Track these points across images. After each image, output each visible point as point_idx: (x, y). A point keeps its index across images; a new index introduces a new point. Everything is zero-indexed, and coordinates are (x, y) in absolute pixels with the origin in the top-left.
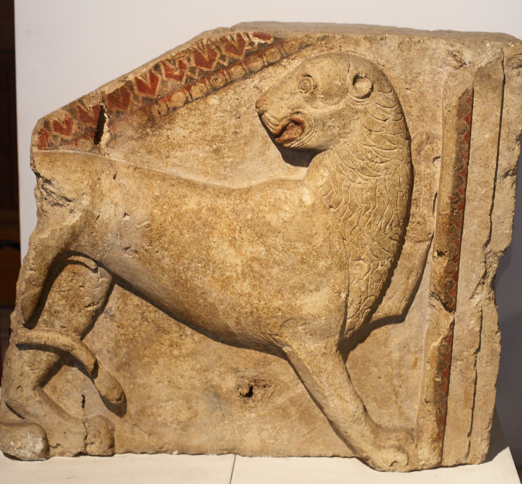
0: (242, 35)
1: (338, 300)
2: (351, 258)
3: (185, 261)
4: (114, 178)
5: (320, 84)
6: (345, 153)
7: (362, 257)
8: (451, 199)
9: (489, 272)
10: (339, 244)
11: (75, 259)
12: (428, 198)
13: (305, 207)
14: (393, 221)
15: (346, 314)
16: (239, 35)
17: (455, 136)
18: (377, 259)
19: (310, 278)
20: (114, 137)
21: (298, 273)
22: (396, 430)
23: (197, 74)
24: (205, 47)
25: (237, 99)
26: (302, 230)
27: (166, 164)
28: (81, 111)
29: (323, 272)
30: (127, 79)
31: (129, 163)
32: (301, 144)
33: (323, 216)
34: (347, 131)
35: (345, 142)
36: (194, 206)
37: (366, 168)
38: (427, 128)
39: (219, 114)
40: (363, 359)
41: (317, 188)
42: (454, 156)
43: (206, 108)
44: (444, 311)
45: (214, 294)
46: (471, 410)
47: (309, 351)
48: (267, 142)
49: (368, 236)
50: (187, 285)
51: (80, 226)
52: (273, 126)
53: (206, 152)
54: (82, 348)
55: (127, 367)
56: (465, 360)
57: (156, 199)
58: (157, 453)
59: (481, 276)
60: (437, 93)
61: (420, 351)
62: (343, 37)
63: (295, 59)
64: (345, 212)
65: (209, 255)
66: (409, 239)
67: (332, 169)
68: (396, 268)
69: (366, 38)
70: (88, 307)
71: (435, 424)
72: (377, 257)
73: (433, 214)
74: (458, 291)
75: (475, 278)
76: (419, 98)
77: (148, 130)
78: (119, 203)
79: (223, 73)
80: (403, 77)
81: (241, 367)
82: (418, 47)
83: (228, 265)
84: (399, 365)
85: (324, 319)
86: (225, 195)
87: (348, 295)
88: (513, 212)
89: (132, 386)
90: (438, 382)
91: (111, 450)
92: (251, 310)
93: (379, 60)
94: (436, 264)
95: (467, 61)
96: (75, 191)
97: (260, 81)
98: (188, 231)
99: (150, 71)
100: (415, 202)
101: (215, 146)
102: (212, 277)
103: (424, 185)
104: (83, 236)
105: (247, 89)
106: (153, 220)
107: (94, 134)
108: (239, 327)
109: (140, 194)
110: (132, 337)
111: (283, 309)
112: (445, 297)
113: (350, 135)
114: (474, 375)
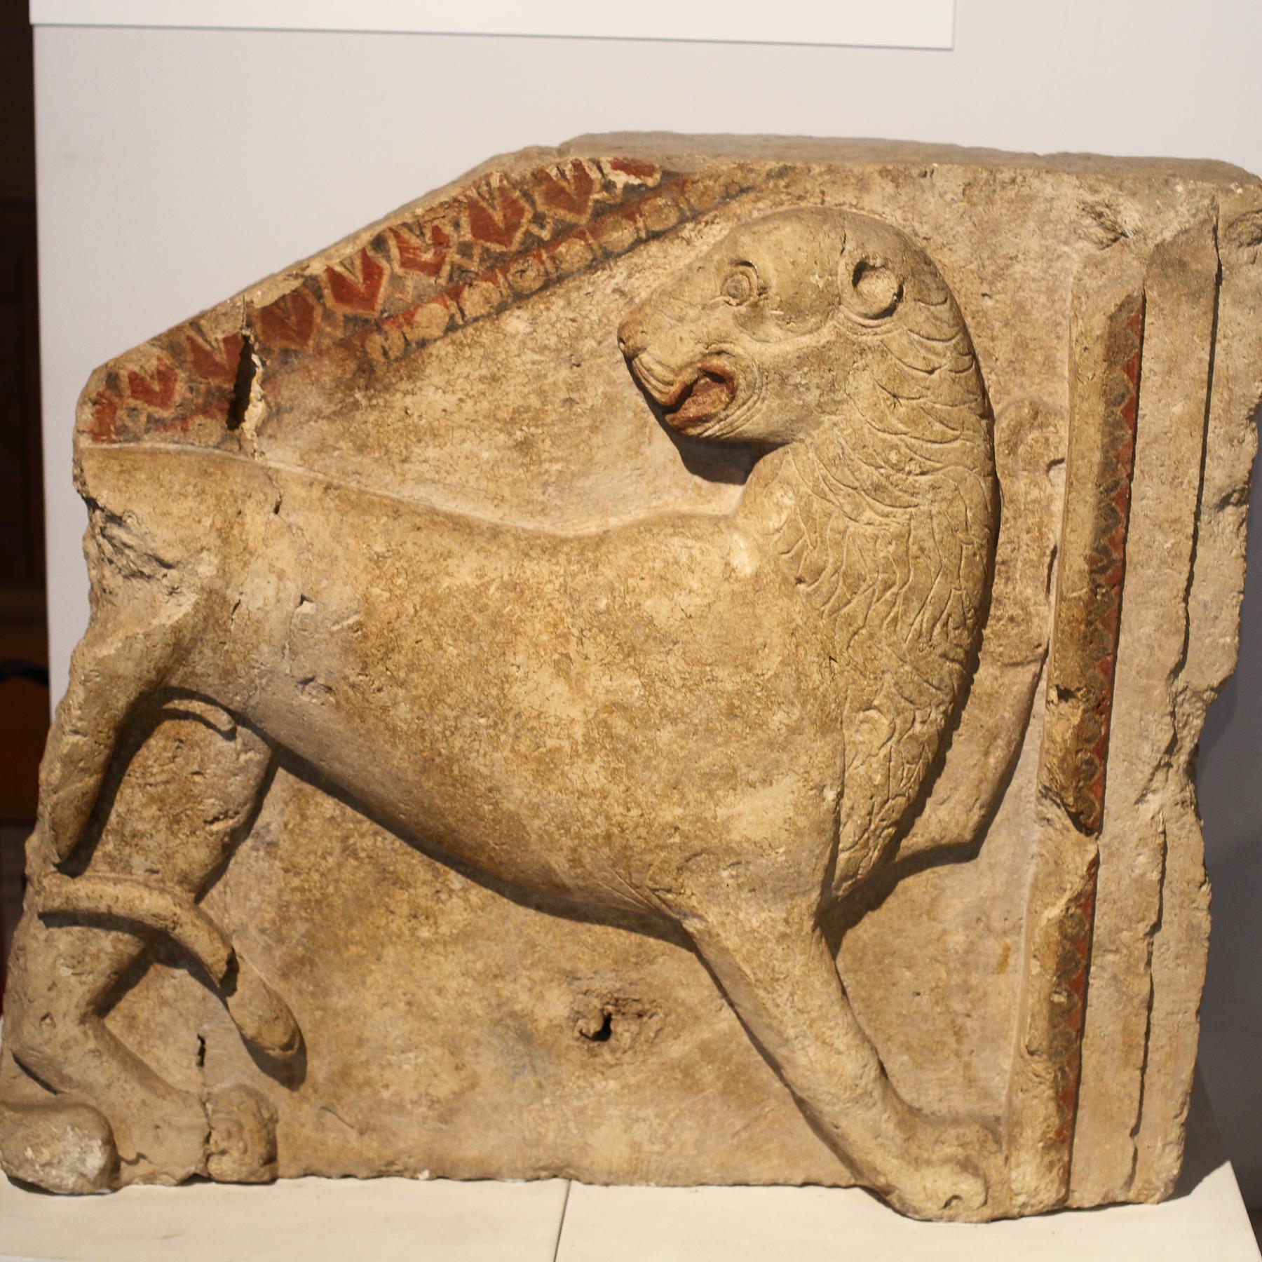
0: (585, 165)
1: (817, 806)
2: (847, 705)
3: (448, 712)
4: (276, 511)
5: (774, 283)
6: (833, 451)
7: (876, 703)
8: (1091, 561)
9: (1182, 739)
10: (820, 671)
11: (182, 708)
12: (1035, 558)
13: (737, 580)
14: (949, 615)
15: (836, 839)
16: (577, 166)
17: (1101, 408)
18: (912, 707)
19: (750, 752)
20: (275, 413)
21: (720, 739)
22: (956, 1121)
23: (476, 258)
24: (497, 194)
25: (573, 320)
26: (730, 637)
27: (400, 478)
28: (196, 348)
29: (781, 739)
30: (307, 273)
31: (313, 474)
32: (729, 429)
33: (780, 603)
34: (839, 396)
35: (835, 424)
36: (469, 580)
37: (885, 487)
38: (1033, 390)
39: (529, 356)
40: (877, 949)
41: (767, 534)
42: (1097, 457)
43: (497, 342)
44: (1074, 833)
45: (518, 793)
46: (1138, 1073)
47: (747, 929)
48: (644, 425)
49: (889, 651)
50: (452, 771)
51: (194, 627)
52: (660, 386)
53: (498, 448)
54: (198, 923)
55: (308, 968)
56: (1125, 951)
57: (376, 563)
58: (380, 1175)
59: (1163, 748)
60: (1057, 306)
61: (1016, 928)
62: (830, 170)
63: (713, 223)
64: (833, 593)
65: (505, 696)
66: (989, 659)
67: (803, 489)
68: (957, 727)
69: (884, 173)
70: (212, 822)
71: (1052, 1106)
72: (911, 702)
73: (1047, 597)
74: (1108, 783)
75: (1149, 752)
76: (1013, 316)
77: (358, 396)
78: (289, 571)
79: (539, 256)
80: (973, 266)
81: (583, 968)
82: (1011, 193)
83: (552, 720)
84: (965, 964)
85: (784, 852)
86: (544, 552)
87: (840, 795)
88: (1240, 592)
89: (318, 1014)
90: (1060, 1004)
91: (268, 1169)
92: (608, 831)
93: (917, 226)
94: (1054, 719)
95: (1128, 228)
96: (182, 541)
97: (630, 276)
98: (455, 640)
99: (363, 251)
100: (1003, 568)
101: (519, 433)
102: (513, 750)
103: (1024, 527)
104: (201, 652)
105: (598, 296)
106: (369, 614)
107: (226, 406)
108: (579, 871)
109: (339, 551)
110: (318, 895)
111: (685, 827)
112: (1076, 800)
113: (845, 406)
114: (1147, 989)
